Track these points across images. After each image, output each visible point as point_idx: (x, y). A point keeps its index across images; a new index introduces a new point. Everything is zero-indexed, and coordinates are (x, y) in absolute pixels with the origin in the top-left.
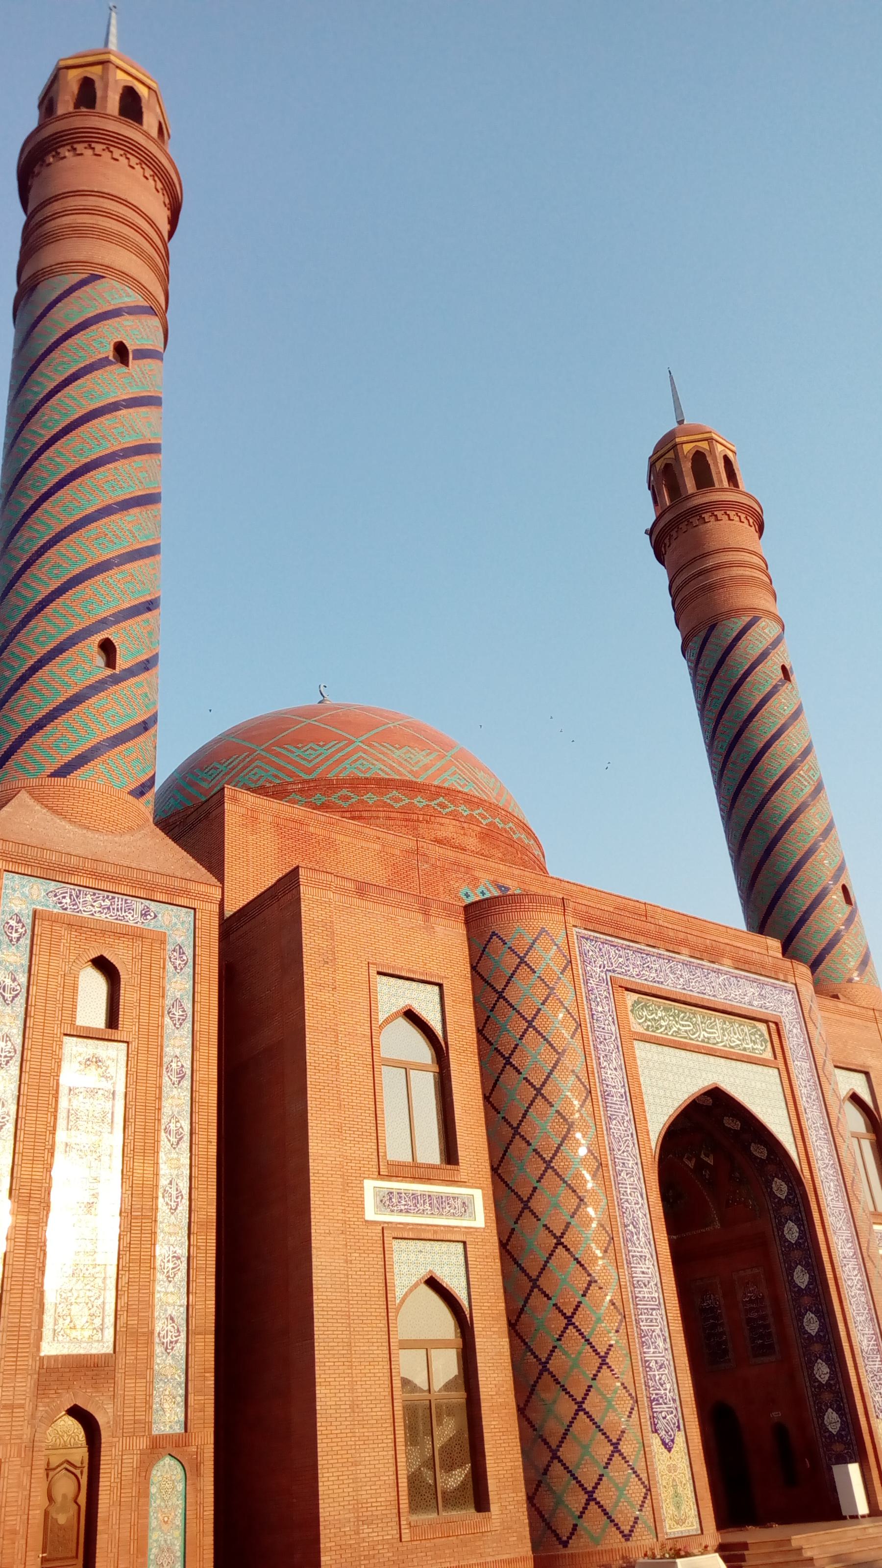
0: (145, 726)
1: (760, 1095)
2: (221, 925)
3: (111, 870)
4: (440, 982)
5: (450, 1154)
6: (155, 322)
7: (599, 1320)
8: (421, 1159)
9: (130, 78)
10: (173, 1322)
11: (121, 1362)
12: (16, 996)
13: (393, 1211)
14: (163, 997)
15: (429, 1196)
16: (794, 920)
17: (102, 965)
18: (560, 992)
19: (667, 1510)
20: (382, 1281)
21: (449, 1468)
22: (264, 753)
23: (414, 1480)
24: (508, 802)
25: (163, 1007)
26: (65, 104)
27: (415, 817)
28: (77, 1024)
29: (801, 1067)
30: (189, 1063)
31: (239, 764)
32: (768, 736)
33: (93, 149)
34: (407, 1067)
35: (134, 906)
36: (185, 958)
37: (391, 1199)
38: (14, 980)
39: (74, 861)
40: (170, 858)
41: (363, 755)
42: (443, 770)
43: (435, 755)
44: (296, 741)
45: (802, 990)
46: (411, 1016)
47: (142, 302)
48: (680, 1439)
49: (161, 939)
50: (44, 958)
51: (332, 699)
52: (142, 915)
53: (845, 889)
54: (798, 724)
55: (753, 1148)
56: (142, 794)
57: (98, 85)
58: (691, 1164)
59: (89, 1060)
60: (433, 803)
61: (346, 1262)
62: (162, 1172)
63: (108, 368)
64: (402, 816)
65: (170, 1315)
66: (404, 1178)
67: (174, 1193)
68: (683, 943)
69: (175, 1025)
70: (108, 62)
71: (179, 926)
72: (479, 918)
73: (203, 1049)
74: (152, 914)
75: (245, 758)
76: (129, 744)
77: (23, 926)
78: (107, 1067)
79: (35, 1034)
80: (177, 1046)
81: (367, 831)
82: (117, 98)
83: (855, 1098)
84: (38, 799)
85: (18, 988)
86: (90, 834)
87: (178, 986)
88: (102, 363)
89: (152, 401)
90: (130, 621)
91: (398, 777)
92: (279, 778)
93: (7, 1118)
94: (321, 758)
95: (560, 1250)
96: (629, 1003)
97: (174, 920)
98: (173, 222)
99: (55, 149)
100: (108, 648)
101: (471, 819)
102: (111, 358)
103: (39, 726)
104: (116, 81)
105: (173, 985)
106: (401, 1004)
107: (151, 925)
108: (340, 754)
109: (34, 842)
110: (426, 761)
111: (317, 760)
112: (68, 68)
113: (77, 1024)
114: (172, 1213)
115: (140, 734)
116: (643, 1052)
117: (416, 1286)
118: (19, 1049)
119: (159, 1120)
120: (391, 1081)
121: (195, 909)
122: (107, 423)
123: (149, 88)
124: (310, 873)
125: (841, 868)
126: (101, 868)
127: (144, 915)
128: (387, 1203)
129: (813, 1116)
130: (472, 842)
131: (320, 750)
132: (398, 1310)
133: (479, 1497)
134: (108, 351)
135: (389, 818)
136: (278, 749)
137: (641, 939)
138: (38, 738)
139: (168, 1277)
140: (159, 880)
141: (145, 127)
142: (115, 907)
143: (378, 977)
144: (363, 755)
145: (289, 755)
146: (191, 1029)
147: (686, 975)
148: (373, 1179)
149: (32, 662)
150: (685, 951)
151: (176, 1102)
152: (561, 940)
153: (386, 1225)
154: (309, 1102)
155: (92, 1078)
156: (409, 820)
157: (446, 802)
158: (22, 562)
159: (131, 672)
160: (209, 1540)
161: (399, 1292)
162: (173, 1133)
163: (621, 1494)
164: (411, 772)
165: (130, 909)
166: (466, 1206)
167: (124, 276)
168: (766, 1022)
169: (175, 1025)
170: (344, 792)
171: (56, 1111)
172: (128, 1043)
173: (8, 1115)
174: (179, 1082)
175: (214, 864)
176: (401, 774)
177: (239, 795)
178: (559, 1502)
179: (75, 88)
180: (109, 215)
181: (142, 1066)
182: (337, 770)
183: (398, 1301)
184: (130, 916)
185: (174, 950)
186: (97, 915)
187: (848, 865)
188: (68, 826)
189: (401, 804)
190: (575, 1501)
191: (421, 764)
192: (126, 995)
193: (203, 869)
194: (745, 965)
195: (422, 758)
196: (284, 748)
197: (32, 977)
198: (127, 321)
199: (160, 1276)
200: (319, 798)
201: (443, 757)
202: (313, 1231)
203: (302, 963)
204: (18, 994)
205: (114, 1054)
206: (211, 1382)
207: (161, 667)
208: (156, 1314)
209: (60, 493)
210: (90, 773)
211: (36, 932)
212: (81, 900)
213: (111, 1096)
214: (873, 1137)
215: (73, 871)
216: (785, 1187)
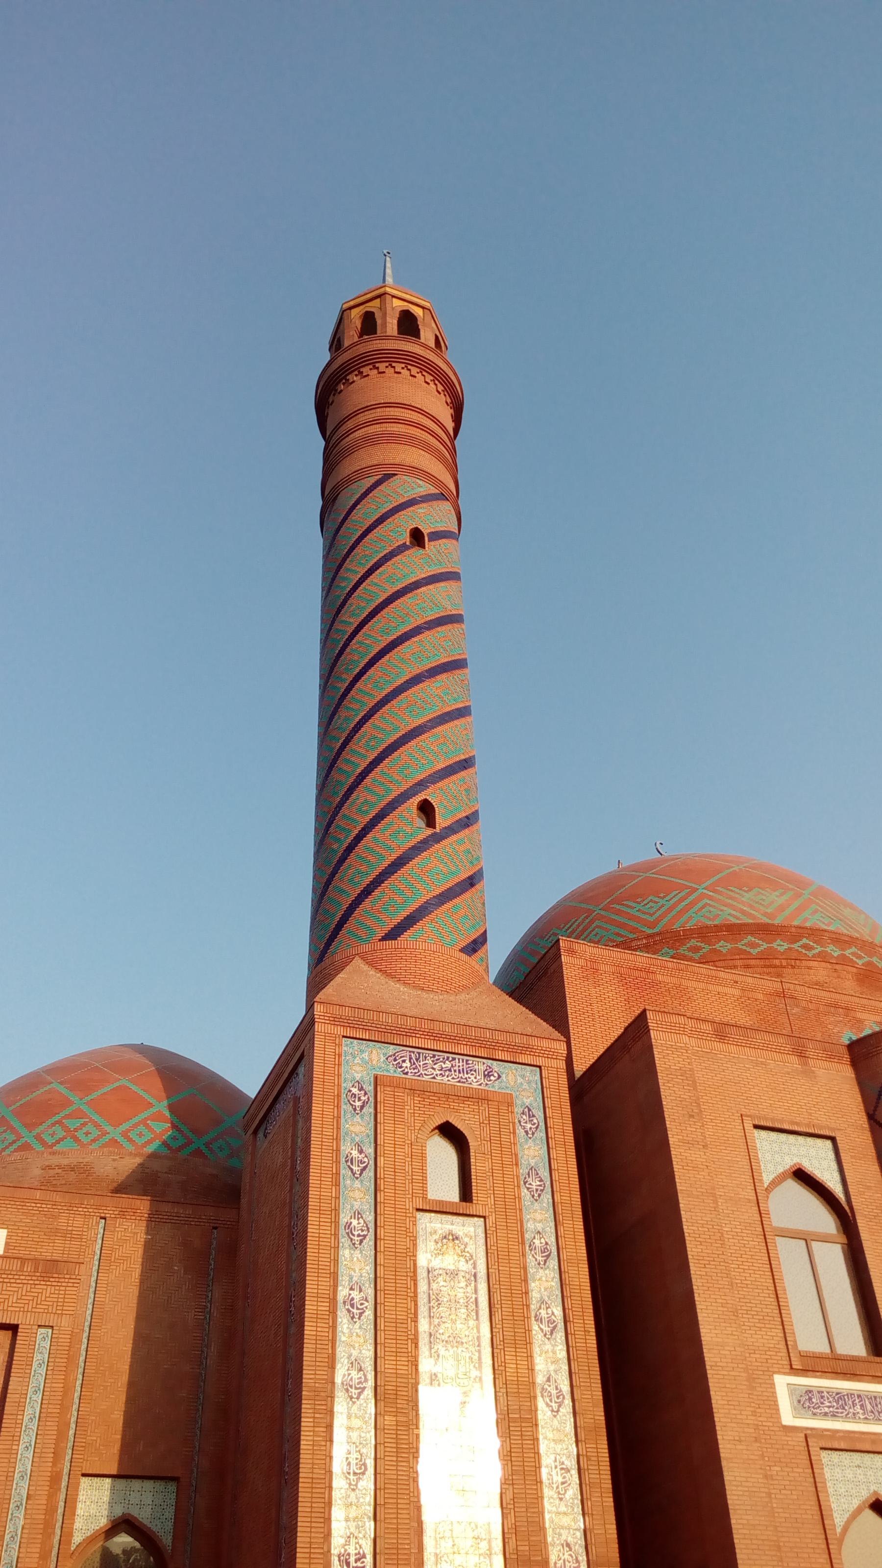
0: (471, 882)
2: (571, 1088)
3: (448, 1029)
4: (833, 1135)
6: (447, 506)
8: (842, 1349)
9: (406, 304)
10: (571, 1550)
12: (365, 1168)
13: (815, 1414)
14: (517, 1164)
15: (859, 1396)
17: (449, 1131)
20: (814, 1502)
22: (603, 913)
25: (518, 1177)
26: (351, 336)
27: (777, 962)
28: (429, 1197)
30: (553, 1239)
31: (579, 926)
33: (378, 368)
34: (807, 1238)
35: (476, 1067)
36: (535, 1121)
37: (810, 1399)
38: (361, 1152)
39: (410, 1022)
41: (708, 902)
42: (800, 910)
43: (789, 894)
46: (801, 1176)
47: (433, 491)
51: (667, 852)
52: (485, 1076)
56: (475, 951)
57: (378, 316)
59: (445, 1237)
60: (795, 946)
61: (766, 1477)
62: (537, 1368)
63: (407, 552)
64: (762, 962)
65: (566, 1541)
67: (554, 1392)
69: (533, 1196)
70: (385, 293)
71: (525, 1086)
73: (568, 1224)
74: (496, 1075)
75: (584, 920)
76: (457, 901)
77: (366, 1094)
78: (466, 1245)
80: (538, 1220)
81: (722, 974)
82: (395, 322)
84: (371, 964)
85: (366, 1160)
86: (425, 995)
87: (532, 1153)
88: (401, 549)
89: (452, 576)
90: (446, 781)
91: (751, 921)
92: (622, 936)
93: (367, 1304)
94: (663, 909)
97: (520, 1080)
98: (457, 419)
99: (345, 378)
100: (426, 809)
101: (843, 961)
102: (408, 543)
103: (367, 892)
104: (393, 309)
105: (526, 1152)
106: (788, 1162)
107: (495, 1086)
108: (684, 904)
110: (781, 901)
111: (660, 912)
112: (350, 308)
113: (429, 1197)
114: (555, 1416)
115: (467, 890)
117: (858, 1511)
118: (371, 1226)
119: (528, 1306)
120: (790, 1255)
121: (540, 1067)
122: (410, 601)
123: (423, 308)
124: (659, 1017)
126: (437, 1027)
128: (807, 1404)
130: (849, 984)
131: (662, 902)
132: (841, 1541)
134: (406, 538)
136: (618, 907)
138: (367, 903)
139: (559, 1493)
141: (422, 340)
142: (457, 1068)
143: (756, 1131)
144: (708, 902)
145: (629, 910)
146: (551, 1201)
148: (785, 1374)
149: (356, 832)
151: (543, 1283)
153: (809, 1432)
154: (693, 1280)
155: (449, 1261)
156: (769, 963)
157: (811, 944)
158: (341, 741)
159: (451, 830)
161: (839, 1519)
162: (545, 1321)
164: (766, 914)
165: (471, 1071)
167: (415, 471)
169: (533, 1196)
170: (693, 943)
171: (416, 1296)
172: (484, 1217)
173: (366, 1300)
174: (545, 1261)
176: (754, 917)
177: (576, 947)
179: (358, 324)
180: (397, 421)
181: (502, 1244)
182: (683, 919)
183: (839, 1530)
184: (472, 1077)
185: (523, 1113)
186: (439, 1078)
189: (759, 949)
191: (775, 905)
193: (545, 1023)
196: (623, 905)
197: (379, 1147)
198: (421, 509)
199: (547, 1492)
201: (798, 896)
202: (719, 1437)
203: (664, 1118)
204: (366, 1166)
205: (469, 1230)
207: (487, 884)
208: (549, 1539)
209: (371, 672)
211: (379, 1100)
212: (422, 1063)
213: (473, 1278)
215: (411, 1033)
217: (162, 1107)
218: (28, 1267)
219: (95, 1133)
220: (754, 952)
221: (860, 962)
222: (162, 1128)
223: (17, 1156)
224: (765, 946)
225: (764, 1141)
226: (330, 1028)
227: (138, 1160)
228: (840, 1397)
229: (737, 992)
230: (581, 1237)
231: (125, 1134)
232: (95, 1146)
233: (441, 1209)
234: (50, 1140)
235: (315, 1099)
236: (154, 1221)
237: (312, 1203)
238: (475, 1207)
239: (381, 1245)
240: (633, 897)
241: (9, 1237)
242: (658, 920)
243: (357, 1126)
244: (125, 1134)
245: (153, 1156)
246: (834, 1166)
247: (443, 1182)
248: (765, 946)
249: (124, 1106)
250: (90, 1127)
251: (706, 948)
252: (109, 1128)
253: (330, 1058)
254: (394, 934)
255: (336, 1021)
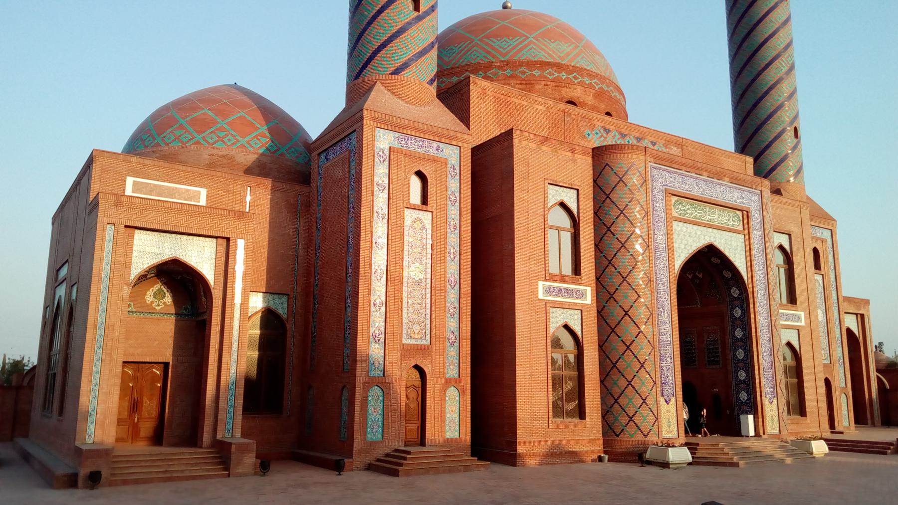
1: (733, 249)
3: (422, 127)
5: (577, 269)
7: (642, 348)
8: (563, 273)
11: (433, 349)
16: (763, 146)
17: (419, 174)
18: (637, 195)
19: (664, 427)
21: (568, 401)
23: (555, 404)
24: (610, 74)
29: (756, 234)
32: (767, 35)
34: (559, 229)
40: (444, 117)
42: (577, 56)
43: (573, 46)
44: (497, 35)
45: (764, 194)
46: (563, 205)
48: (673, 400)
49: (445, 162)
50: (395, 171)
53: (796, 129)
54: (786, 28)
55: (724, 272)
58: (690, 277)
66: (556, 281)
68: (705, 170)
72: (600, 155)
73: (465, 216)
79: (393, 207)
80: (453, 212)
83: (781, 247)
95: (626, 317)
96: (673, 202)
101: (590, 86)
103: (384, 45)
106: (558, 199)
107: (441, 155)
109: (389, 113)
110: (568, 50)
116: (677, 226)
120: (552, 235)
125: (796, 117)
126: (418, 125)
127: (437, 150)
129: (758, 259)
130: (590, 100)
131: (511, 42)
133: (581, 413)
135: (546, 85)
137: (683, 168)
140: (444, 132)
147: (704, 187)
149: (378, 8)
150: (705, 174)
151: (453, 239)
152: (642, 170)
160: (469, 419)
163: (645, 419)
164: (559, 57)
166: (583, 295)
168: (742, 211)
170: (523, 68)
175: (465, 118)
176: (554, 58)
178: (616, 419)
187: (794, 41)
188: (401, 103)
190: (624, 420)
192: (431, 190)
194: (736, 180)
195: (565, 48)
200: (509, 72)
201: (577, 47)
205: (426, 217)
206: (469, 359)
210: (410, 73)
214: (787, 266)
216: (737, 292)
217: (264, 129)
218: (232, 214)
219: (233, 140)
220: (551, 77)
221: (597, 87)
222: (266, 141)
223: (193, 147)
224: (557, 75)
225: (551, 190)
226: (369, 122)
227: (256, 156)
228: (560, 289)
229: (545, 109)
230: (470, 222)
231: (248, 142)
232: (234, 147)
233: (414, 208)
234: (211, 141)
235: (364, 157)
236: (274, 190)
237: (363, 202)
238: (429, 208)
239: (390, 222)
240: (496, 36)
241: (208, 192)
242: (507, 53)
243: (381, 170)
244: (248, 142)
245: (262, 155)
246: (576, 201)
247: (415, 197)
248: (557, 75)
249: (245, 127)
250: (230, 137)
251: (529, 73)
252: (239, 138)
253: (370, 138)
254: (397, 72)
255: (372, 119)
